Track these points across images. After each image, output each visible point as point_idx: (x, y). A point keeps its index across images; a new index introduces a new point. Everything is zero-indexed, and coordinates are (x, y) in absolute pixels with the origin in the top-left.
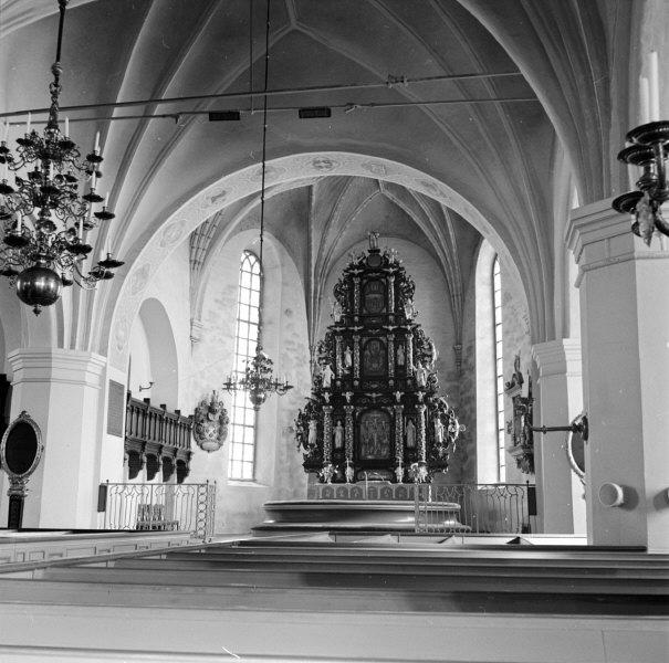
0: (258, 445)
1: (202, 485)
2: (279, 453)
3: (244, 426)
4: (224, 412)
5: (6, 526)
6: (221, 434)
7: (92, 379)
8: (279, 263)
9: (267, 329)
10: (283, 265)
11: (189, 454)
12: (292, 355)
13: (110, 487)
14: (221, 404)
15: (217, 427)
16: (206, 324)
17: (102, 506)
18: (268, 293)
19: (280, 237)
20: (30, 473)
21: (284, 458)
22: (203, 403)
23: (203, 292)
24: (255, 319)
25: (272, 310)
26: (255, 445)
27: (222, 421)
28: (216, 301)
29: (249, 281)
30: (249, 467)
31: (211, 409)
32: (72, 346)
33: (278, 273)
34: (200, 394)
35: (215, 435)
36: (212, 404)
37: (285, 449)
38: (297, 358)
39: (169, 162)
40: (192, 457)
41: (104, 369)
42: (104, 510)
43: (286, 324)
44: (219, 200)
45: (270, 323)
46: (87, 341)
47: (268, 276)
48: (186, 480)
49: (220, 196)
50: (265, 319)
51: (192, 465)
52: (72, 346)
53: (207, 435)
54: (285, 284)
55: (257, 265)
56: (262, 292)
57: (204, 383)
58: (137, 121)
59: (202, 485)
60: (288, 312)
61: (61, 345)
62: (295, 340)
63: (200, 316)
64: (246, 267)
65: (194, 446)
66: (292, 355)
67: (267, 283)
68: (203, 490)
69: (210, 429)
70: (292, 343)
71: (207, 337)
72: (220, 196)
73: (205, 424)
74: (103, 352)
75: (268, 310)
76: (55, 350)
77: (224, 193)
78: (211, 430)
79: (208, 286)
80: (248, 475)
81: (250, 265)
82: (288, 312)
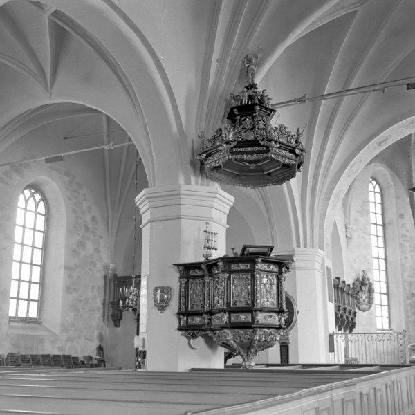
0: (391, 305)
1: (400, 334)
2: (406, 311)
3: (381, 293)
4: (370, 284)
5: (279, 362)
6: (370, 300)
7: (318, 266)
8: (392, 183)
9: (389, 228)
10: (395, 185)
11: (355, 313)
12: (407, 245)
13: (335, 335)
14: (368, 279)
15: (367, 295)
16: (354, 228)
17: (332, 349)
18: (386, 204)
19: (391, 167)
20: (292, 328)
21: (410, 314)
22: (357, 280)
23: (350, 206)
24: (380, 222)
25: (391, 215)
26: (389, 305)
27: (371, 291)
28: (358, 212)
29: (374, 197)
30: (386, 320)
31: (363, 283)
32: (305, 246)
33: (392, 191)
34: (354, 274)
35: (367, 300)
36: (363, 280)
37: (409, 308)
38: (410, 246)
39: (353, 124)
40: (357, 315)
41: (323, 259)
42: (333, 351)
43: (400, 225)
44: (382, 144)
45: (390, 224)
46: (313, 242)
47: (386, 193)
48: (355, 331)
49: (384, 141)
50: (387, 221)
51: (357, 320)
52: (305, 246)
53: (361, 300)
54: (397, 198)
55: (377, 187)
56: (382, 204)
57: (356, 266)
58: (307, 105)
59: (400, 334)
60: (401, 216)
61: (299, 246)
62: (407, 234)
63: (349, 222)
64: (371, 188)
65: (357, 310)
66: (407, 245)
67: (385, 198)
68: (401, 336)
69: (364, 297)
70: (406, 236)
71: (355, 235)
72: (384, 141)
73: (360, 293)
74: (321, 248)
75: (388, 215)
76: (296, 249)
77: (387, 139)
78: (364, 297)
79: (352, 203)
80: (386, 326)
81: (373, 188)
82: (401, 216)
